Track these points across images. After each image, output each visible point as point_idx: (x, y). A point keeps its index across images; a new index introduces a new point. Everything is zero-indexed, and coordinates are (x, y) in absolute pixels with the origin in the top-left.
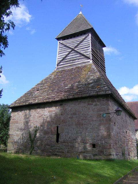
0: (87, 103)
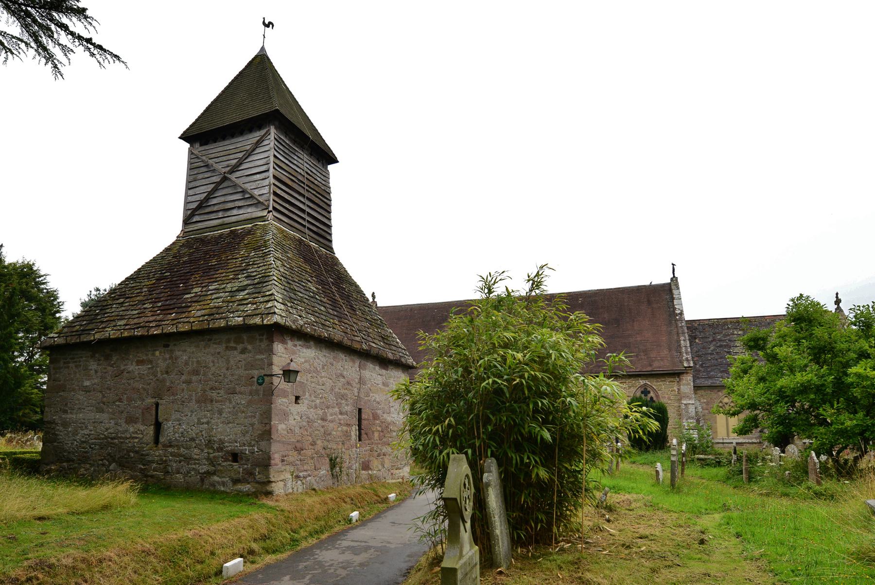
0: (224, 345)
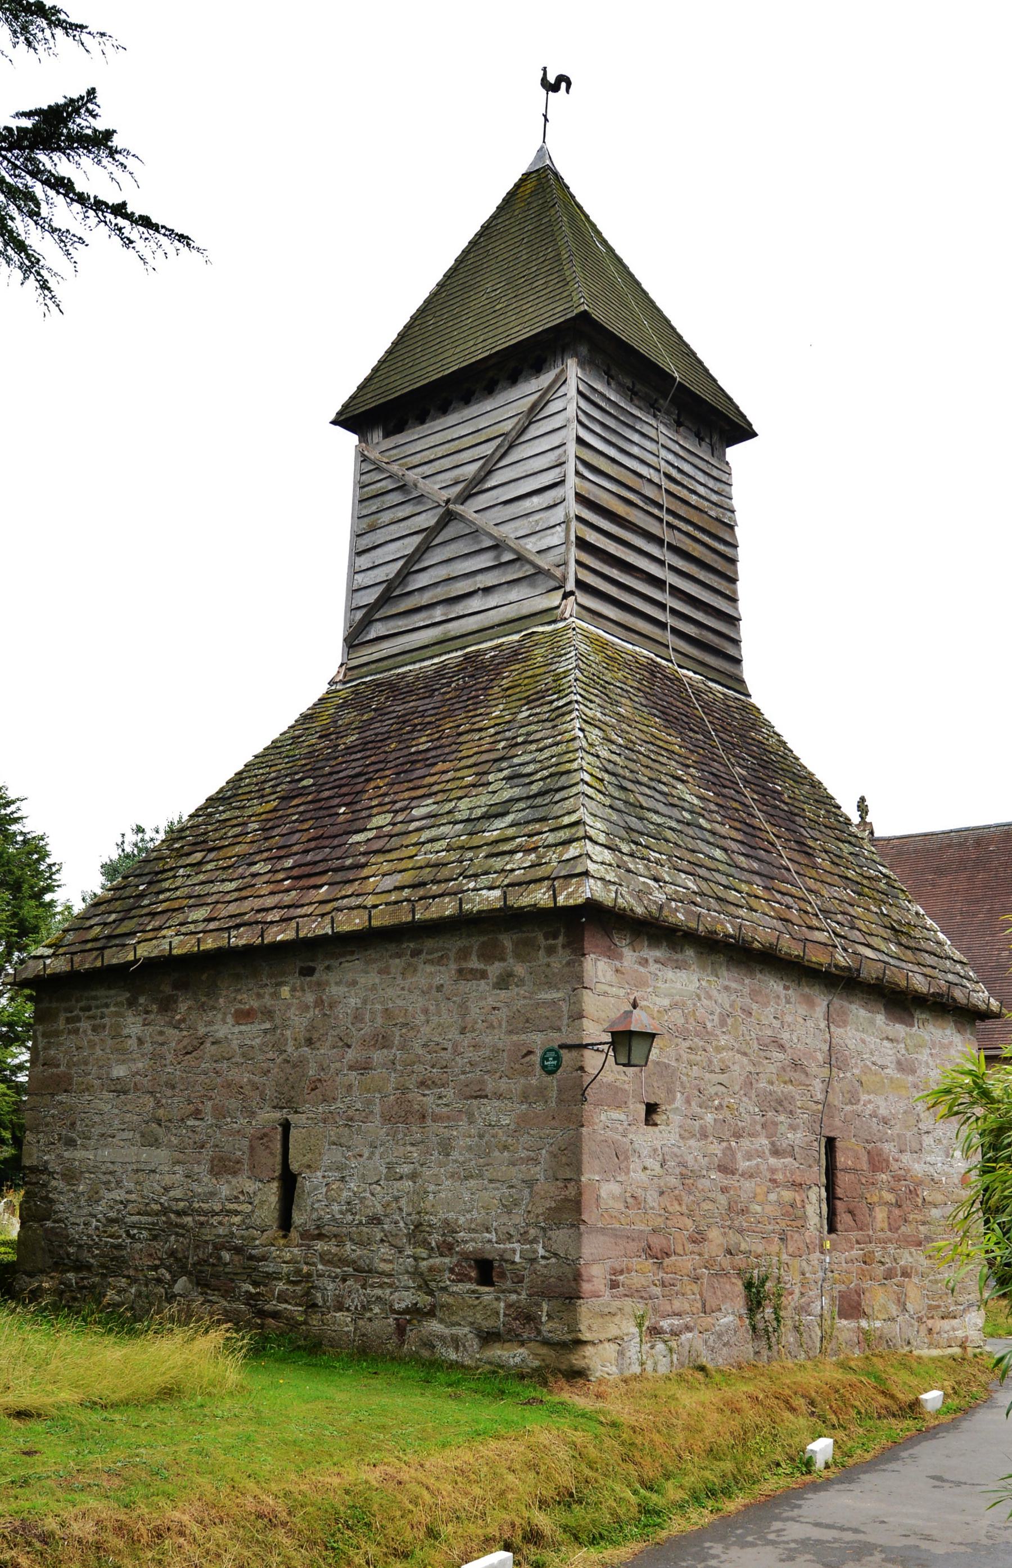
0: (453, 966)
